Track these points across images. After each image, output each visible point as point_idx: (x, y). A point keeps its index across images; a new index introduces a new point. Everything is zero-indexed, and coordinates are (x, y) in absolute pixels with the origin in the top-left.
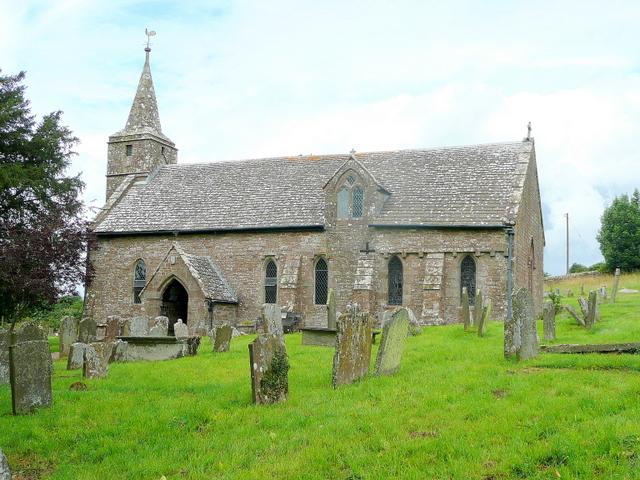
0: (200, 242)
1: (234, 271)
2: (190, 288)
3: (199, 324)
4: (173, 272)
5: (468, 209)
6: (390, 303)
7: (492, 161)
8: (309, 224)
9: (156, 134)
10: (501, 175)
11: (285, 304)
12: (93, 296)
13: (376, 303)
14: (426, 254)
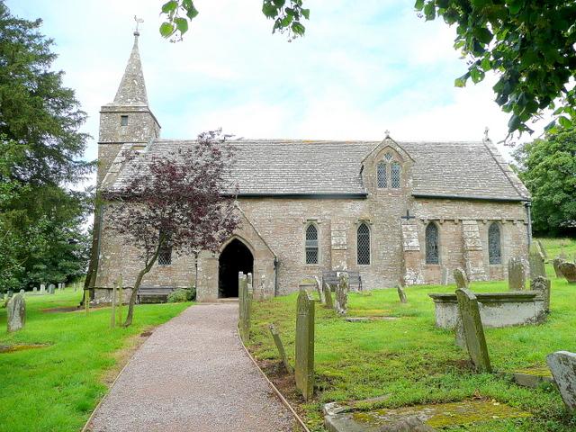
11: (339, 264)
12: (108, 257)
14: (461, 221)
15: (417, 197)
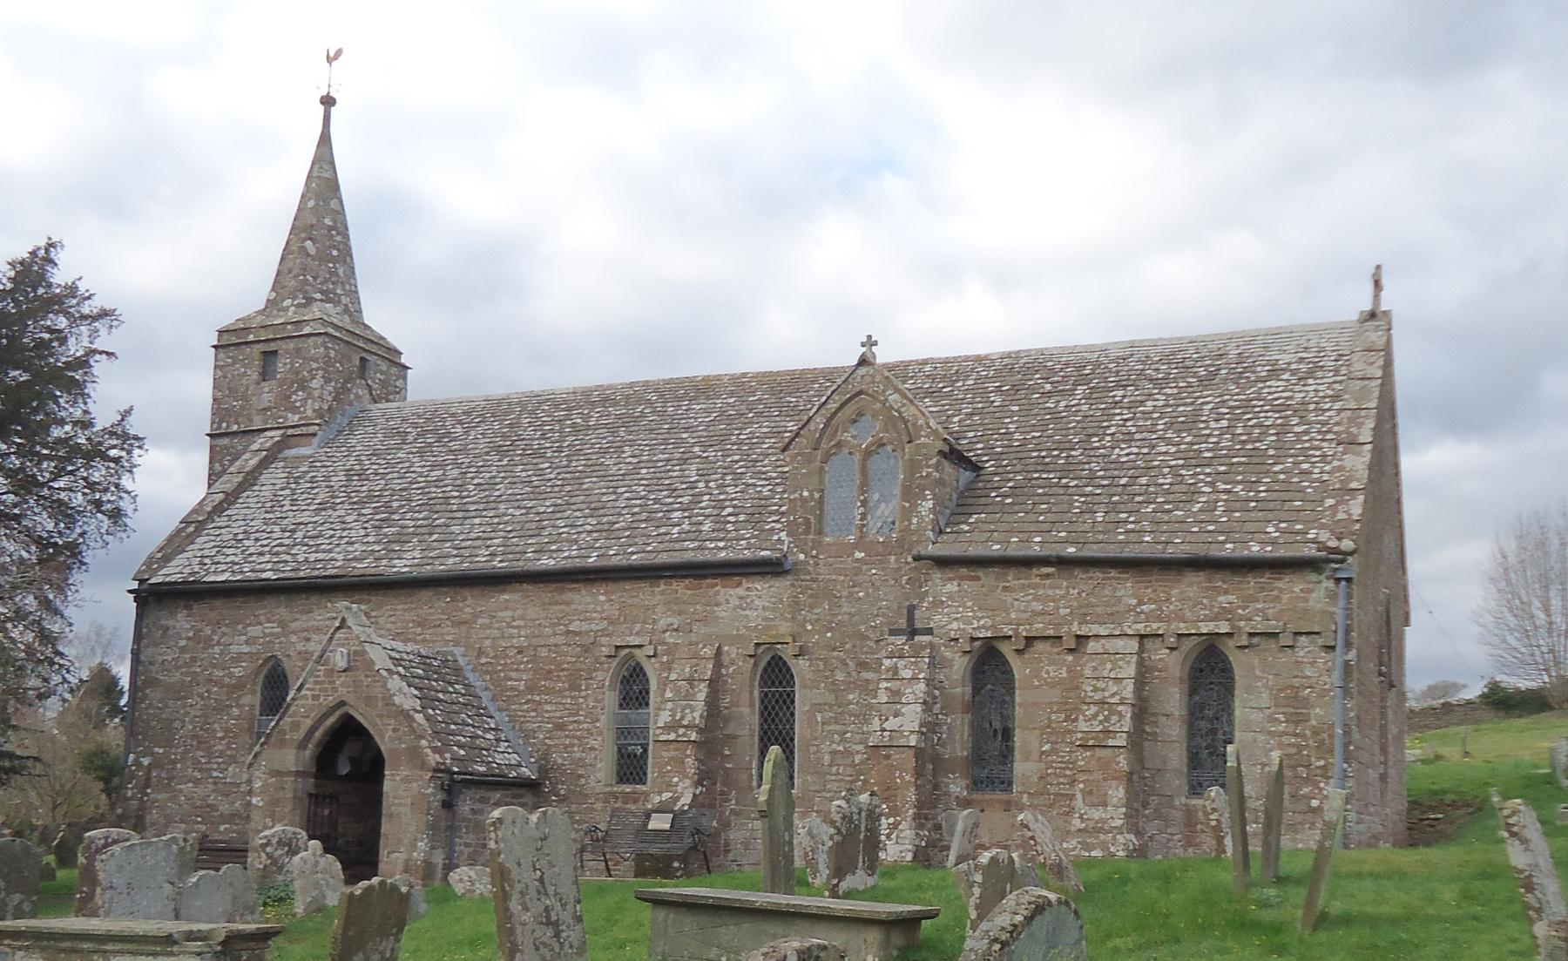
0: (435, 606)
1: (531, 689)
2: (387, 739)
3: (414, 847)
4: (342, 693)
5: (1210, 507)
6: (976, 784)
7: (1275, 373)
8: (744, 552)
9: (346, 322)
10: (1301, 411)
11: (670, 786)
12: (146, 761)
13: (936, 787)
15: (943, 562)
